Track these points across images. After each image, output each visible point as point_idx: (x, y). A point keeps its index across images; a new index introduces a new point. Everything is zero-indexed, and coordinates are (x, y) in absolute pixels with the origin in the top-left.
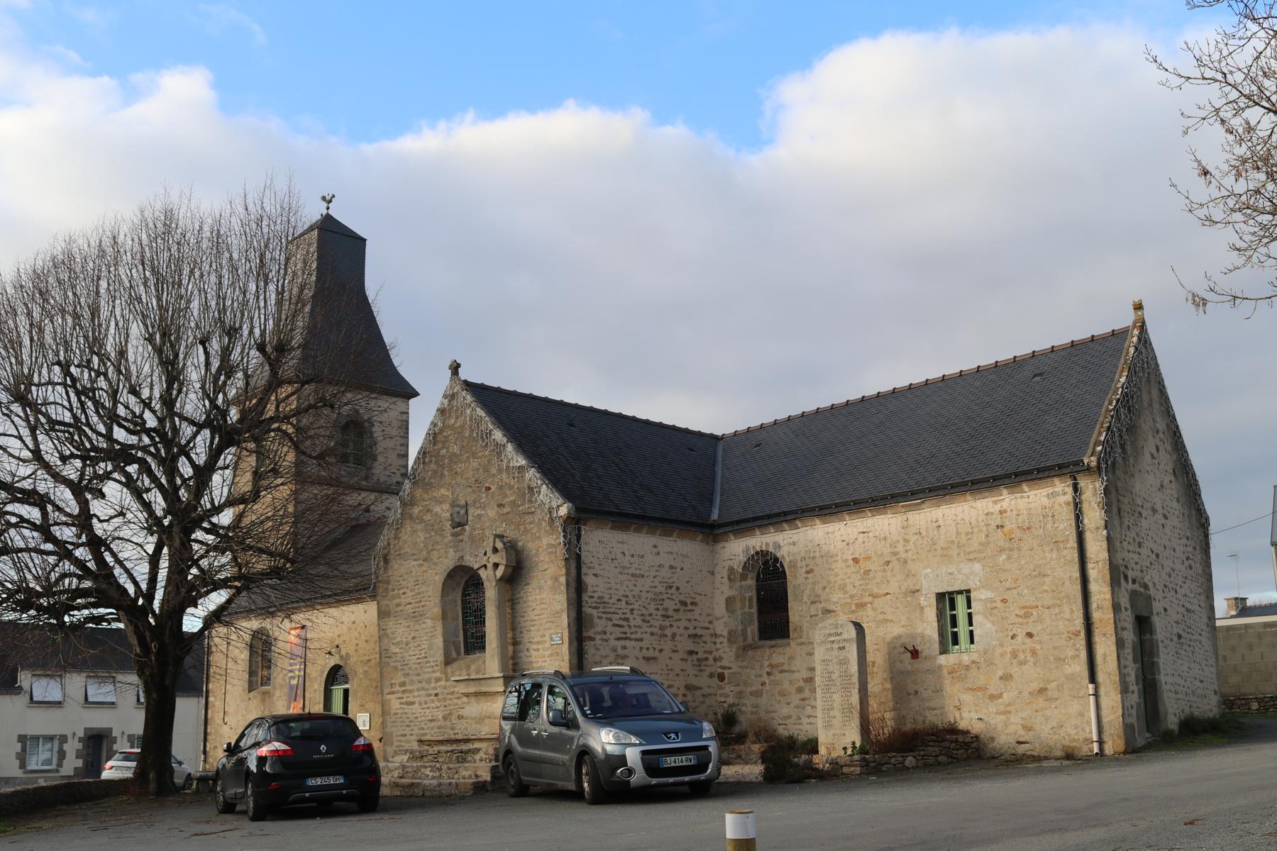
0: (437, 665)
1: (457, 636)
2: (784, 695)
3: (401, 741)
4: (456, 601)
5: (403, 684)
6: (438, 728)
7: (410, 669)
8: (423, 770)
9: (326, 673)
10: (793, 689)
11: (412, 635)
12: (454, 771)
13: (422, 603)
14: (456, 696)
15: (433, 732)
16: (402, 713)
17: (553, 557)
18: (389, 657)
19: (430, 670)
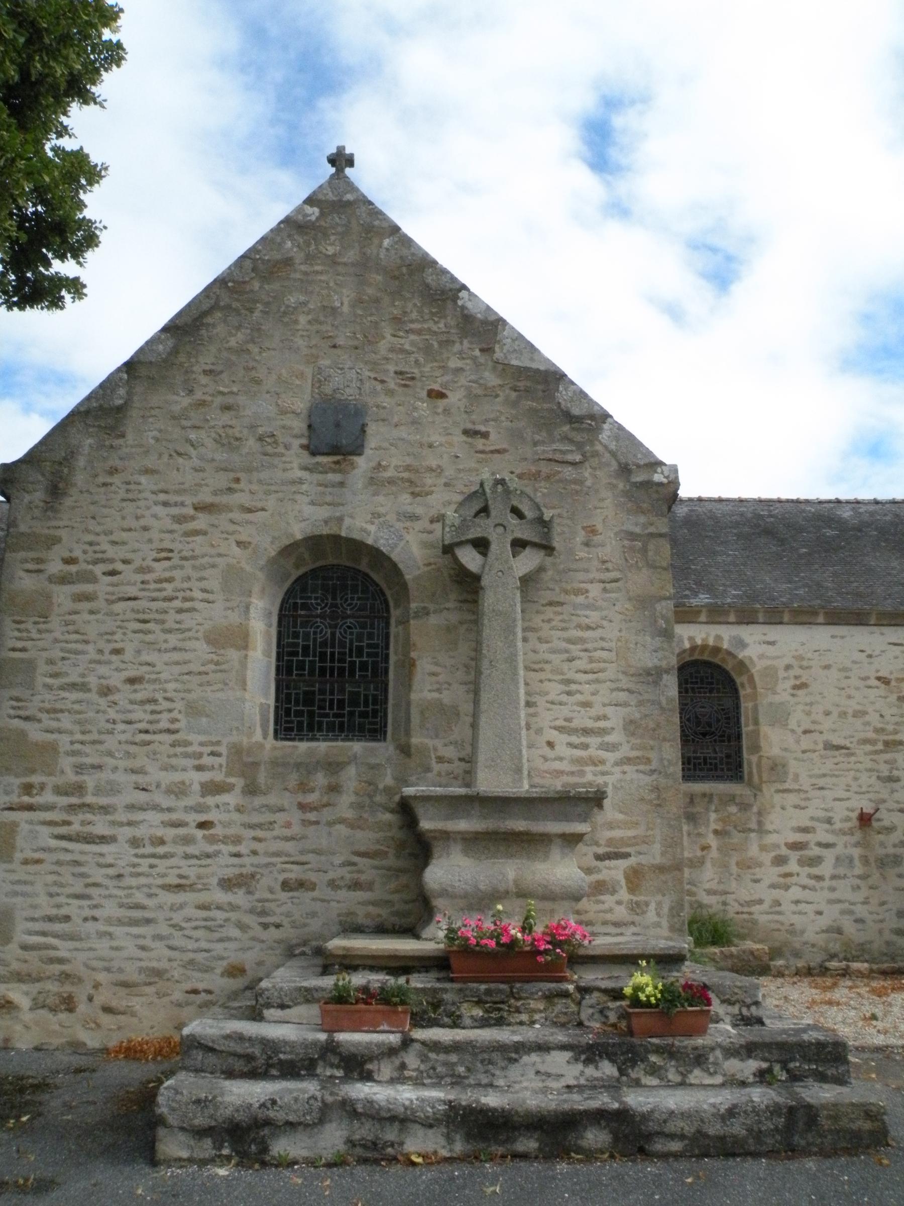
2: (749, 867)
10: (767, 858)
13: (177, 604)
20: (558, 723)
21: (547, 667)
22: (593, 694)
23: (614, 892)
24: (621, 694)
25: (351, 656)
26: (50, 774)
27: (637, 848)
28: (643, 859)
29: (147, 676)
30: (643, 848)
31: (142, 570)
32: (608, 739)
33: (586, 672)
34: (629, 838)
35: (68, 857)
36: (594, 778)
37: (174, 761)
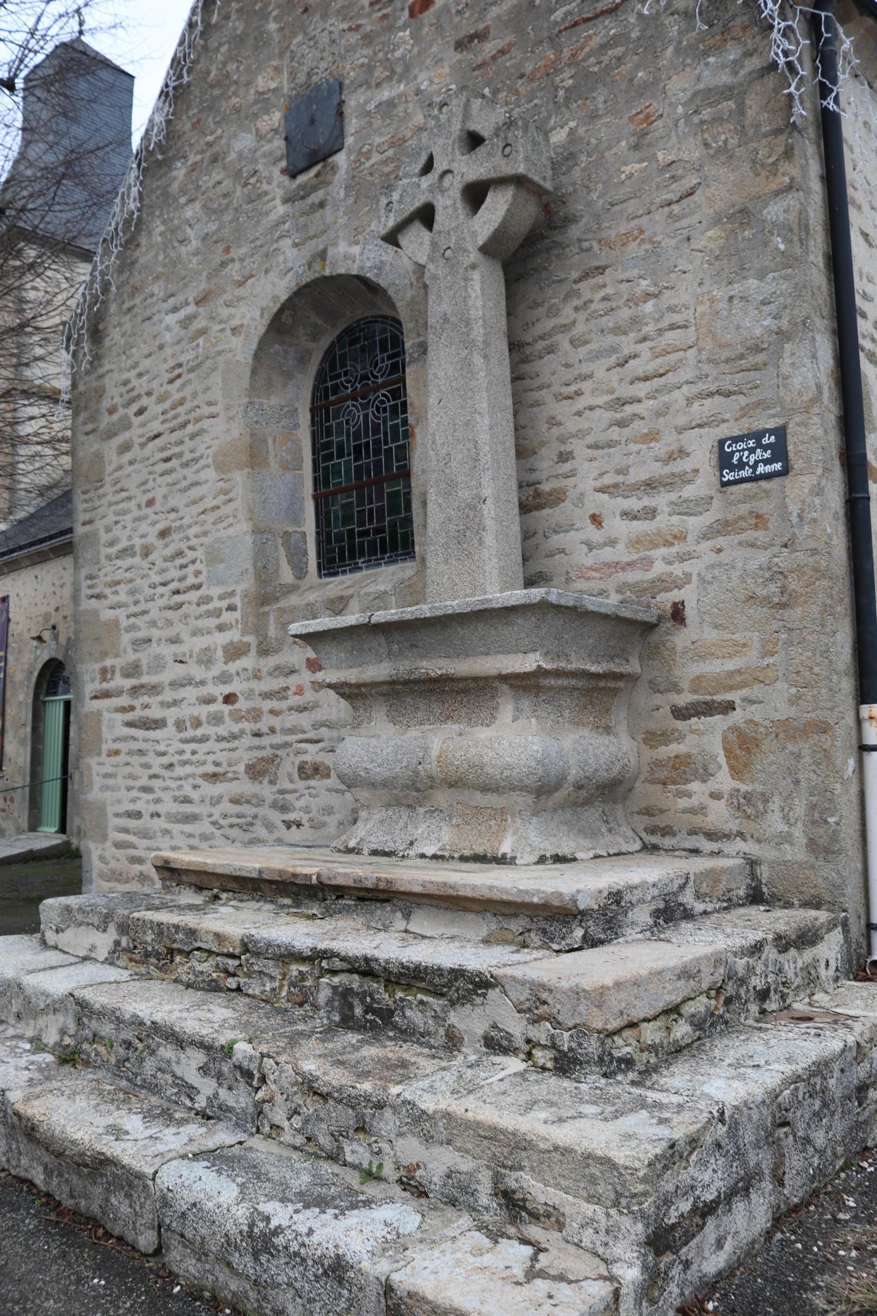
0: (231, 608)
1: (296, 518)
3: (126, 831)
4: (294, 412)
5: (133, 670)
6: (235, 801)
7: (153, 624)
8: (167, 1052)
9: (36, 674)
11: (160, 526)
12: (346, 1117)
13: (190, 429)
14: (294, 700)
15: (217, 811)
16: (130, 753)
17: (725, 135)
18: (98, 597)
19: (212, 622)
20: (608, 480)
21: (586, 386)
22: (659, 414)
23: (706, 775)
24: (708, 402)
25: (386, 443)
26: (117, 656)
27: (745, 692)
28: (755, 712)
29: (174, 525)
30: (756, 691)
31: (161, 399)
32: (689, 492)
33: (646, 379)
34: (731, 674)
35: (134, 746)
36: (669, 569)
37: (200, 623)
